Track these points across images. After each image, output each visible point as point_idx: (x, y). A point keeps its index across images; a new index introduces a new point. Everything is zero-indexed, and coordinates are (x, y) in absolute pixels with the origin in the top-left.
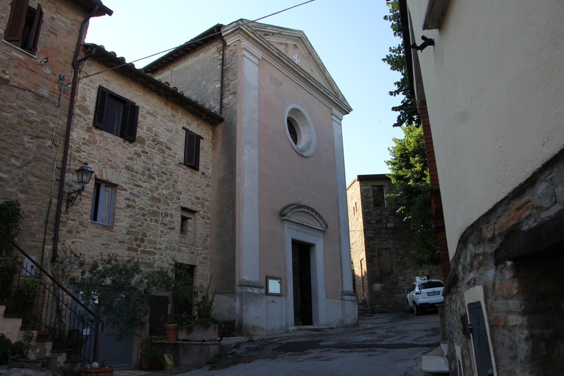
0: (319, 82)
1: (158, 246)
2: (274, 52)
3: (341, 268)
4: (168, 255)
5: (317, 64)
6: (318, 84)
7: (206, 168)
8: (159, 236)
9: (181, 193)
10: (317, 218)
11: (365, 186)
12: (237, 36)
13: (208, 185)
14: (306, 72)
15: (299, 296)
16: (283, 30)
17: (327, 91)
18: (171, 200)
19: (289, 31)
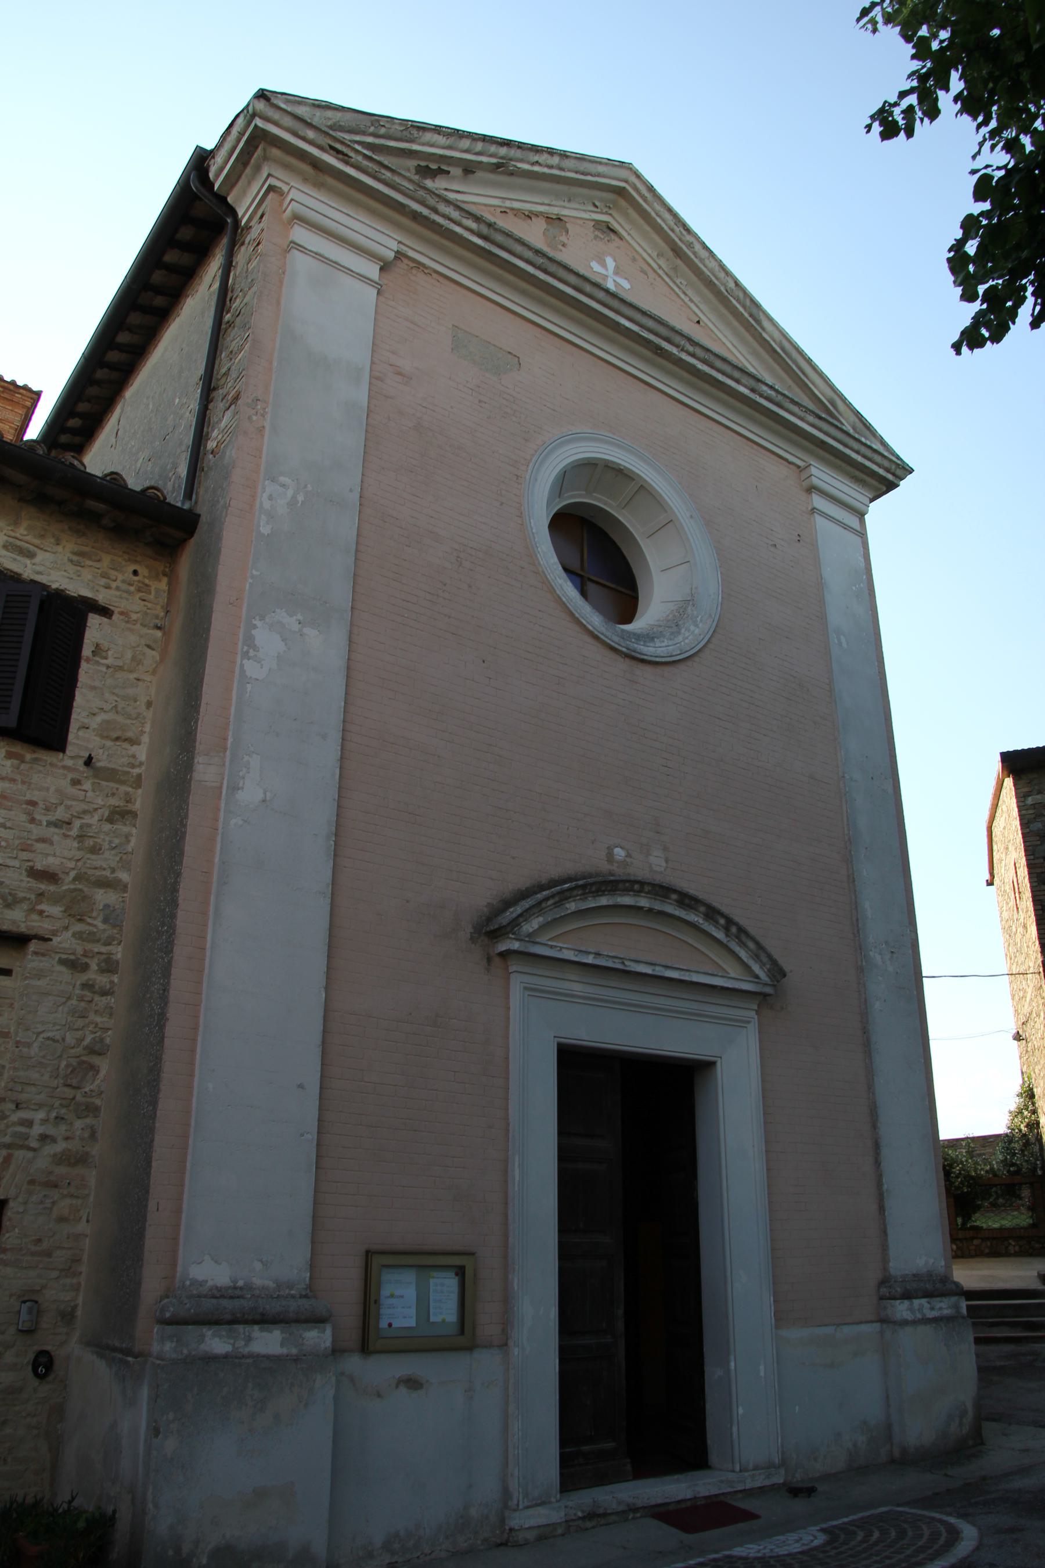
0: (740, 365)
2: (458, 229)
3: (877, 1163)
5: (717, 293)
6: (719, 364)
7: (117, 739)
10: (720, 935)
11: (1039, 792)
12: (265, 175)
13: (119, 815)
14: (644, 313)
15: (620, 1326)
16: (513, 153)
17: (772, 393)
19: (555, 160)
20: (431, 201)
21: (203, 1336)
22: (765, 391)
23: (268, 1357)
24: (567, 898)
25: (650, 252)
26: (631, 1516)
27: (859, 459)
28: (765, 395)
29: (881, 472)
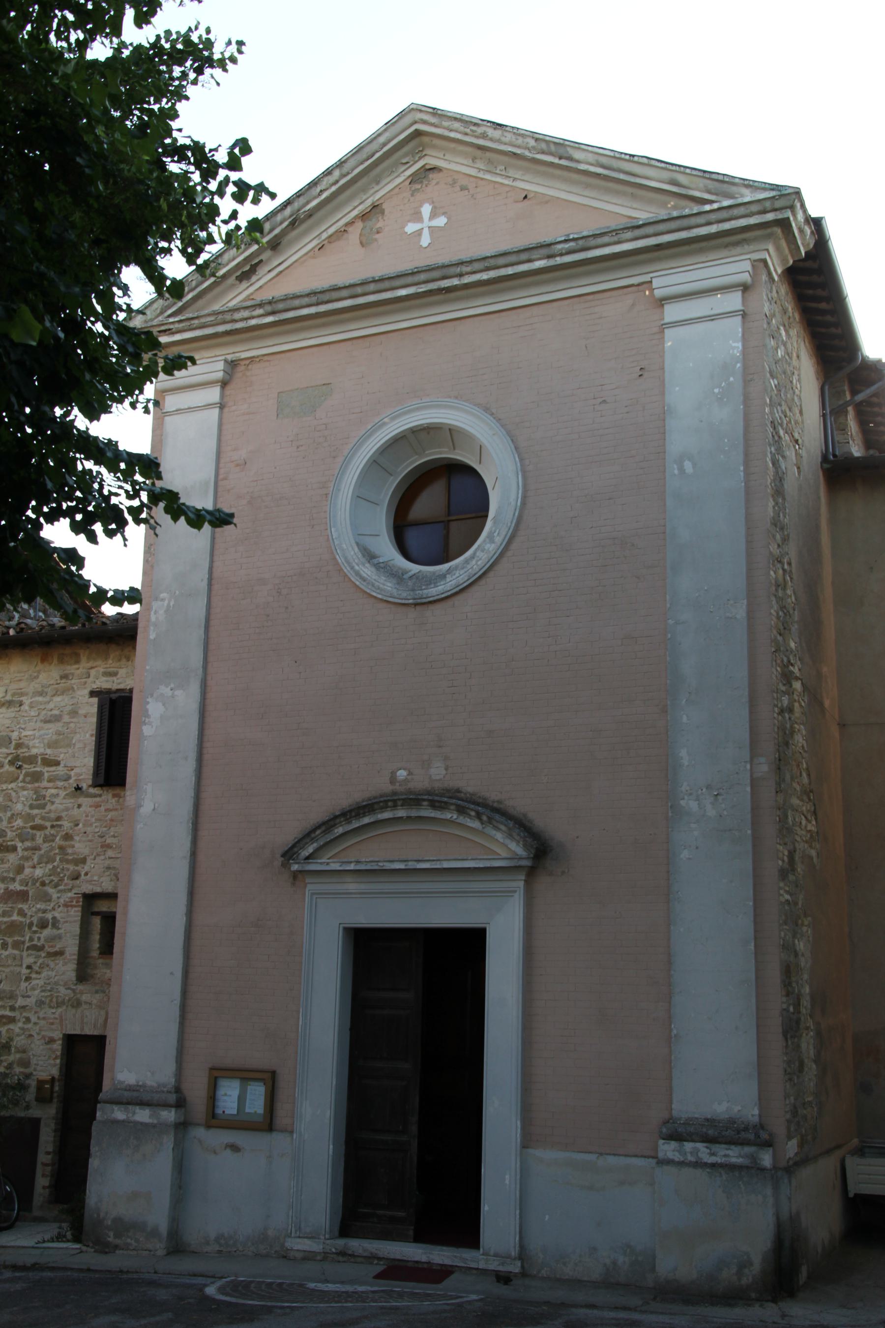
1: (20, 1002)
4: (44, 1018)
6: (501, 261)
8: (24, 978)
9: (84, 861)
15: (414, 1129)
17: (572, 244)
18: (56, 886)
20: (228, 317)
21: (113, 1110)
22: (562, 249)
23: (141, 1123)
24: (335, 825)
25: (465, 162)
26: (376, 1262)
27: (714, 229)
28: (564, 251)
29: (752, 221)
